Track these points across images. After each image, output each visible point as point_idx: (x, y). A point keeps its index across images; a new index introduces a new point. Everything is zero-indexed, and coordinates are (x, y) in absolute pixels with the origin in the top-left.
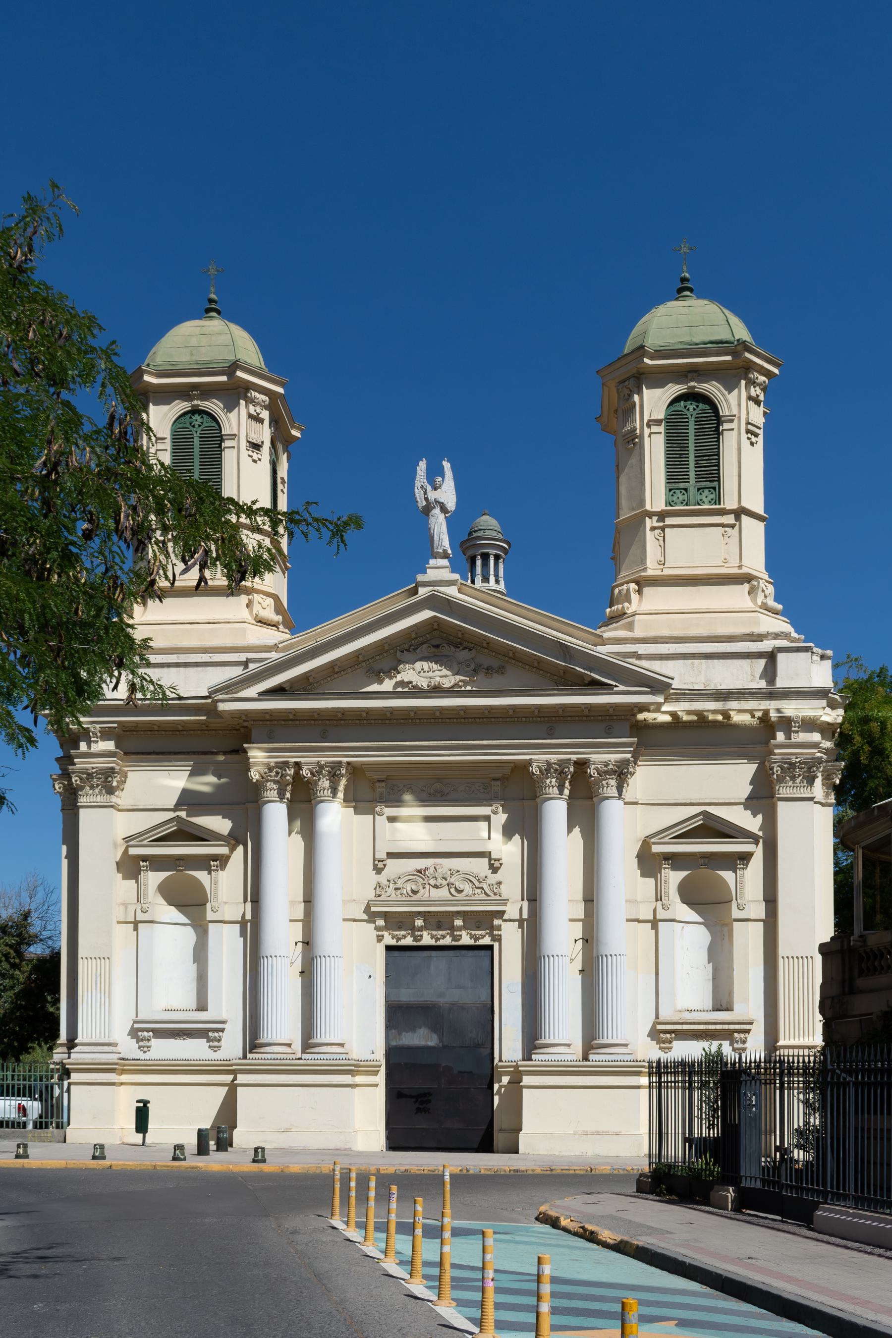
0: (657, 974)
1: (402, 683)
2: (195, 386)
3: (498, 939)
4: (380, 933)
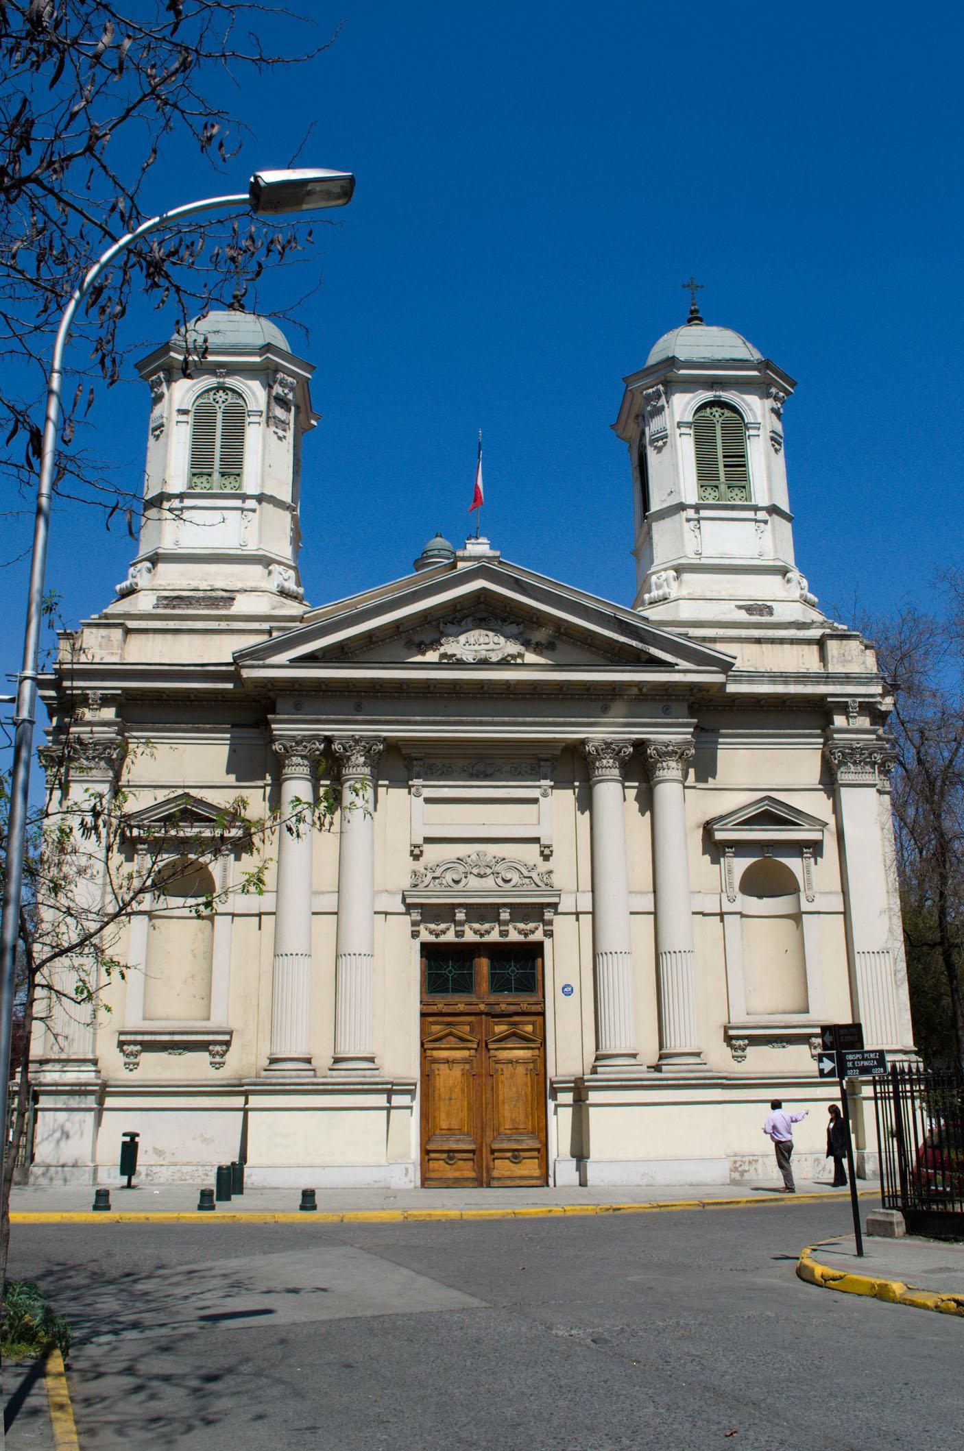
0: (819, 913)
1: (443, 656)
3: (549, 934)
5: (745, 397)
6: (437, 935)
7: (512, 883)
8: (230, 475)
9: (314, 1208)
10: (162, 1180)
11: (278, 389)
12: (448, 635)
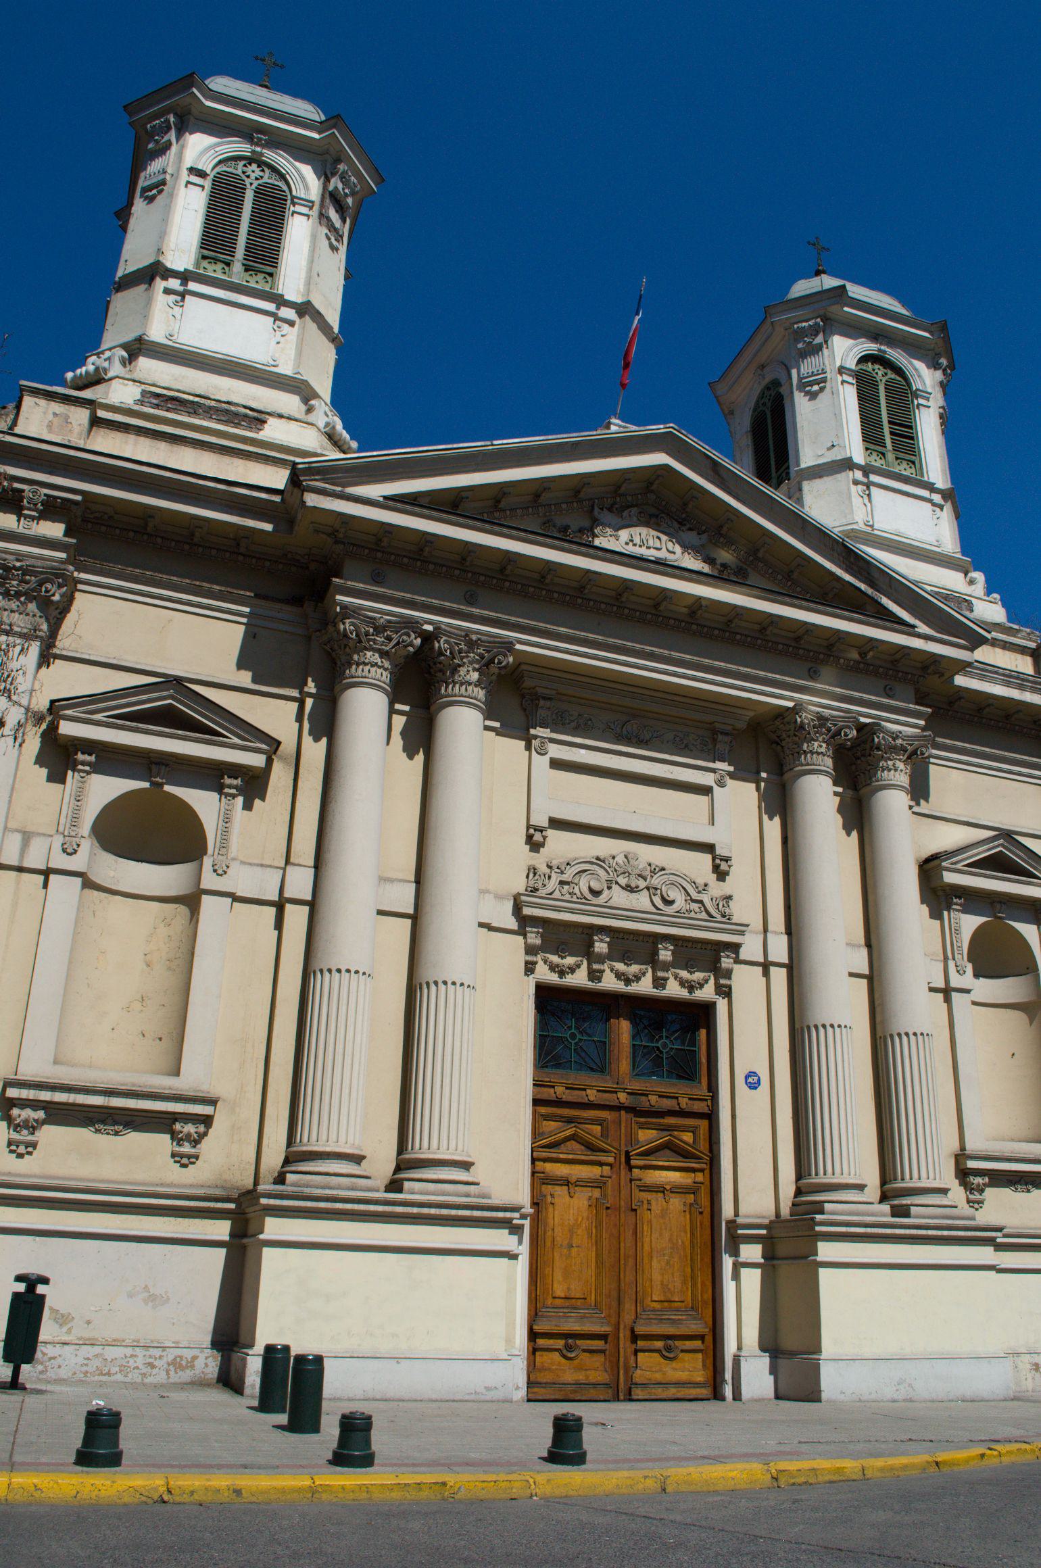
4: (529, 958)
6: (562, 974)
7: (675, 907)
8: (258, 271)
10: (64, 1373)
12: (604, 525)
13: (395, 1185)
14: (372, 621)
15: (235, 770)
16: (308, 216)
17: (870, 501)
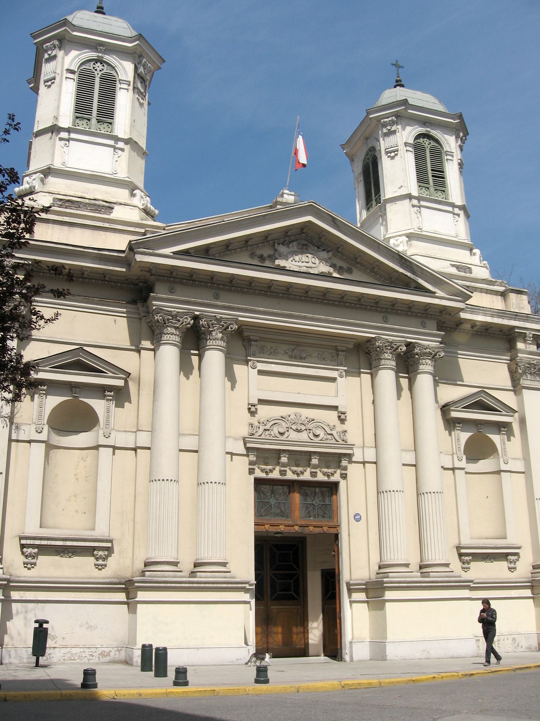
2: (101, 44)
3: (344, 476)
4: (251, 467)
5: (445, 136)
7: (320, 438)
8: (104, 122)
9: (267, 681)
11: (141, 70)
13: (193, 574)
14: (169, 313)
15: (110, 388)
16: (127, 89)
17: (421, 216)
